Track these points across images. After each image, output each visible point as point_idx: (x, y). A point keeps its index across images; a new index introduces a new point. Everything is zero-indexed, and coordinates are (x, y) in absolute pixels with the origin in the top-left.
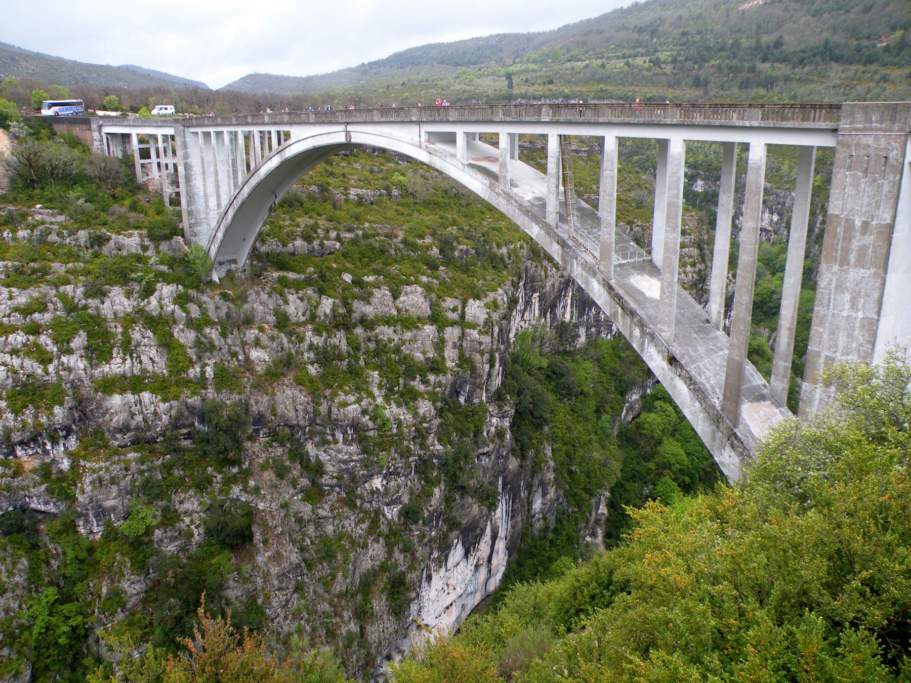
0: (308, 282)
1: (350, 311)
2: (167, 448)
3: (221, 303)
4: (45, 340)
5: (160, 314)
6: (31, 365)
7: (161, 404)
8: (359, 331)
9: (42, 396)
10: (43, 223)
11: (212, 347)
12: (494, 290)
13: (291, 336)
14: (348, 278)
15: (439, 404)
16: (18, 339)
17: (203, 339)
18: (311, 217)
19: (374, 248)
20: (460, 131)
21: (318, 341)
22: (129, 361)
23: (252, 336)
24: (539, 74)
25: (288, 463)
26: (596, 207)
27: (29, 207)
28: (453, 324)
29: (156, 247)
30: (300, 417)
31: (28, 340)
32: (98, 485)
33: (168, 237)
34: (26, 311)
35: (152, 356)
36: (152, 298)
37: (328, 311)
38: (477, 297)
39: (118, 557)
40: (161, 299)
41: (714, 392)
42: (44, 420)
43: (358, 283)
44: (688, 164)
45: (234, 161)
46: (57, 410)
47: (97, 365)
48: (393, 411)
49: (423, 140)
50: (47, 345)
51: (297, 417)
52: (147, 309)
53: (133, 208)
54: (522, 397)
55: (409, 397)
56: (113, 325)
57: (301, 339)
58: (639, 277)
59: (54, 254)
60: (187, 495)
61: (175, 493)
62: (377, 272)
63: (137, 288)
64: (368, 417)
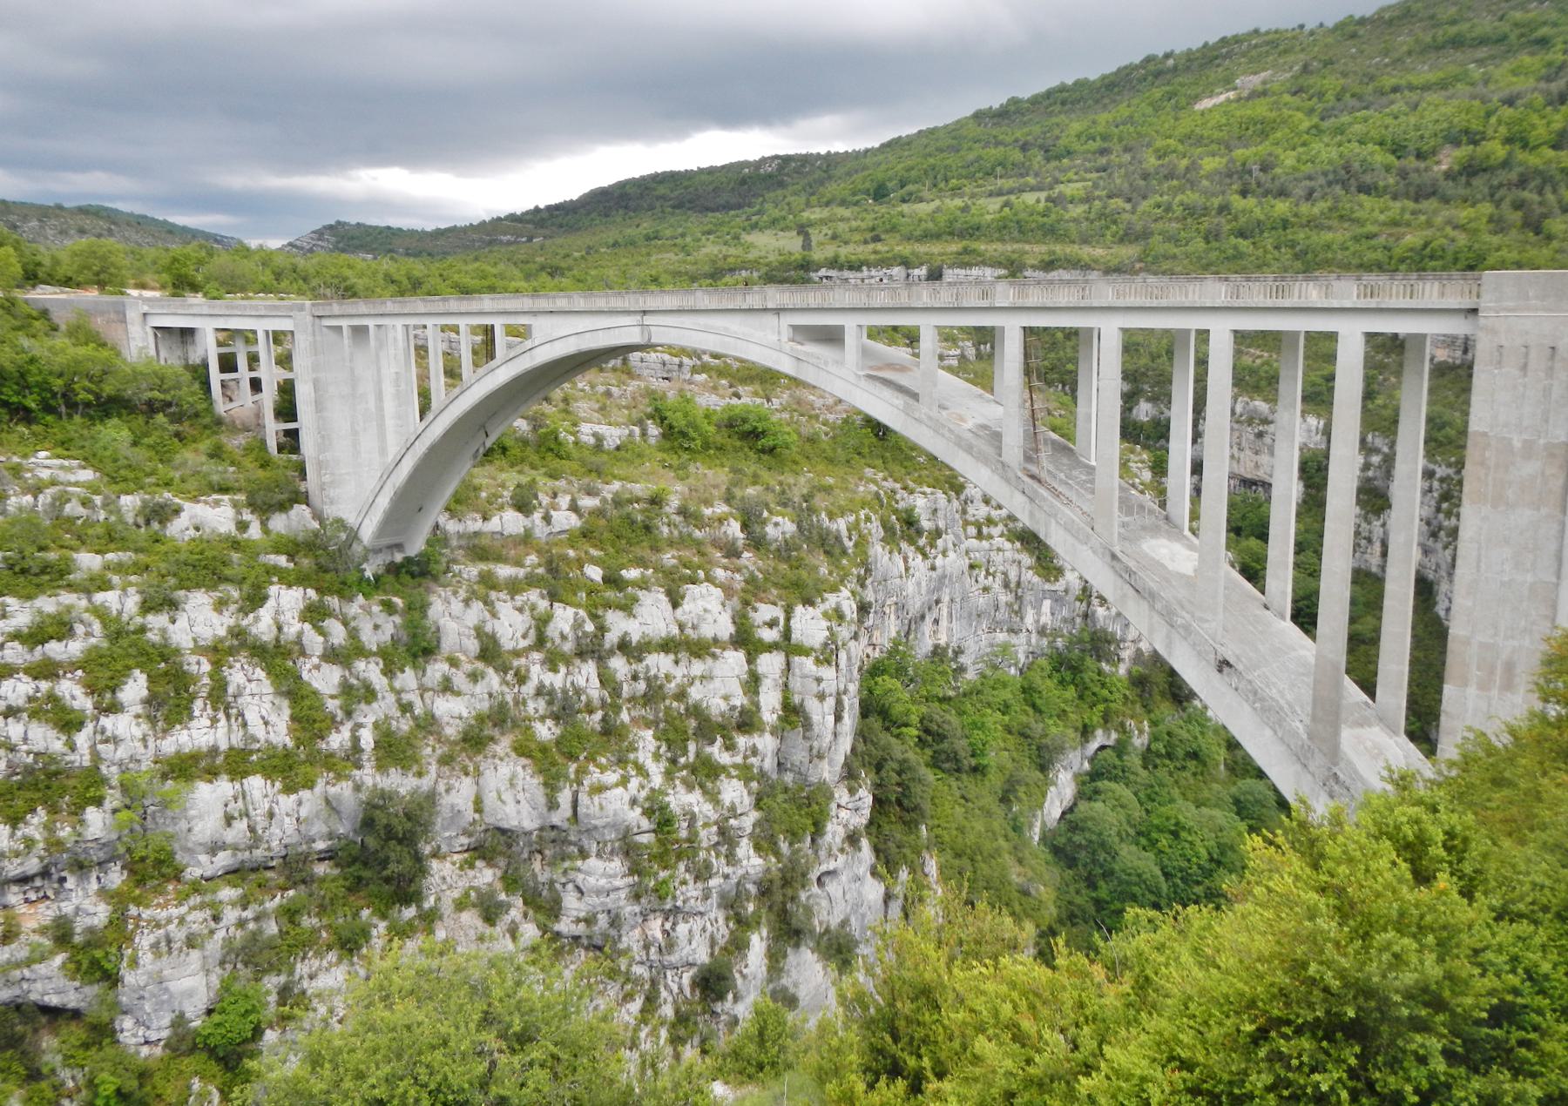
0: (531, 581)
1: (602, 629)
2: (288, 878)
3: (382, 618)
4: (71, 691)
5: (277, 640)
6: (44, 737)
7: (282, 798)
8: (619, 665)
9: (64, 790)
10: (53, 483)
11: (370, 694)
12: (834, 589)
13: (505, 673)
14: (595, 573)
15: (754, 785)
16: (18, 689)
17: (354, 681)
18: (520, 472)
19: (633, 522)
20: (850, 323)
21: (556, 680)
22: (223, 722)
23: (438, 676)
24: (854, 224)
25: (503, 897)
26: (1069, 437)
27: (25, 456)
28: (772, 647)
29: (264, 524)
30: (525, 813)
31: (37, 690)
32: (164, 948)
33: (283, 507)
34: (34, 637)
35: (264, 713)
36: (262, 611)
37: (567, 629)
38: (809, 602)
39: (196, 1085)
40: (277, 612)
41: (1294, 712)
42: (65, 832)
43: (612, 581)
44: (1126, 376)
45: (423, 377)
46: (92, 813)
47: (165, 731)
48: (682, 799)
49: (785, 338)
50: (73, 698)
51: (519, 812)
52: (254, 630)
53: (216, 454)
54: (883, 774)
55: (705, 774)
56: (193, 659)
57: (522, 679)
58: (1154, 542)
59: (79, 538)
60: (325, 963)
61: (303, 959)
62: (641, 563)
63: (235, 594)
64: (638, 810)
